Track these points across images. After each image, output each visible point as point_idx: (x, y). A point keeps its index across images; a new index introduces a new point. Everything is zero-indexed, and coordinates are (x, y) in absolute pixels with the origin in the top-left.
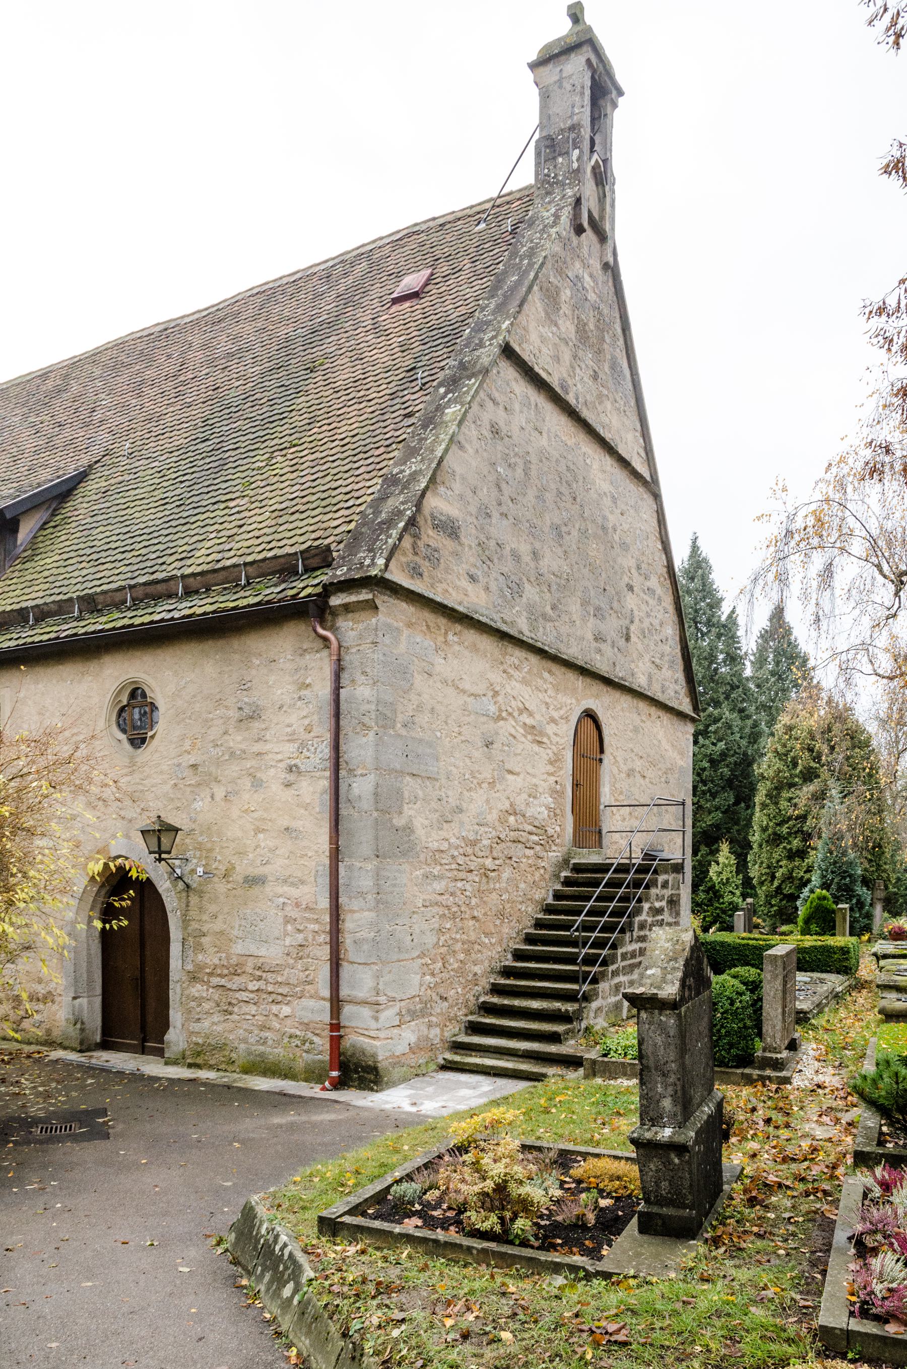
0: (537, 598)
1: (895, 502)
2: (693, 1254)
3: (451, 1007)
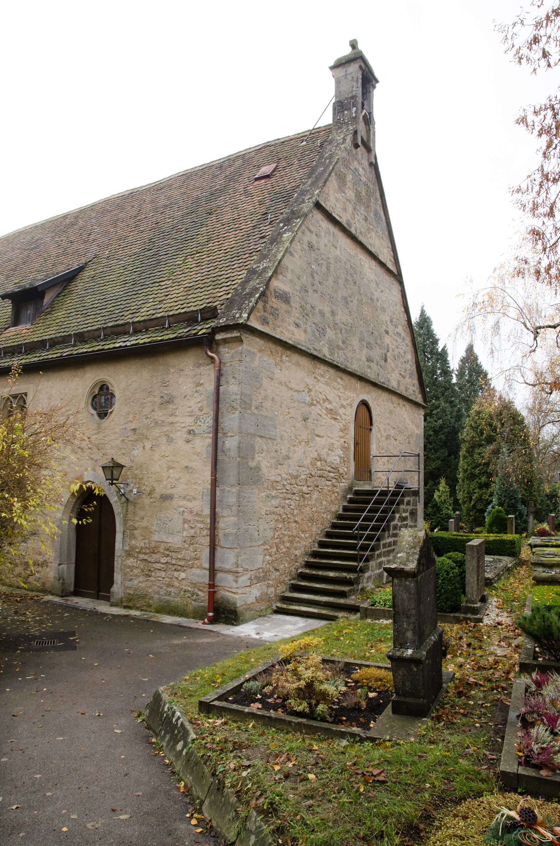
0: (334, 337)
1: (531, 289)
2: (425, 727)
3: (281, 575)
